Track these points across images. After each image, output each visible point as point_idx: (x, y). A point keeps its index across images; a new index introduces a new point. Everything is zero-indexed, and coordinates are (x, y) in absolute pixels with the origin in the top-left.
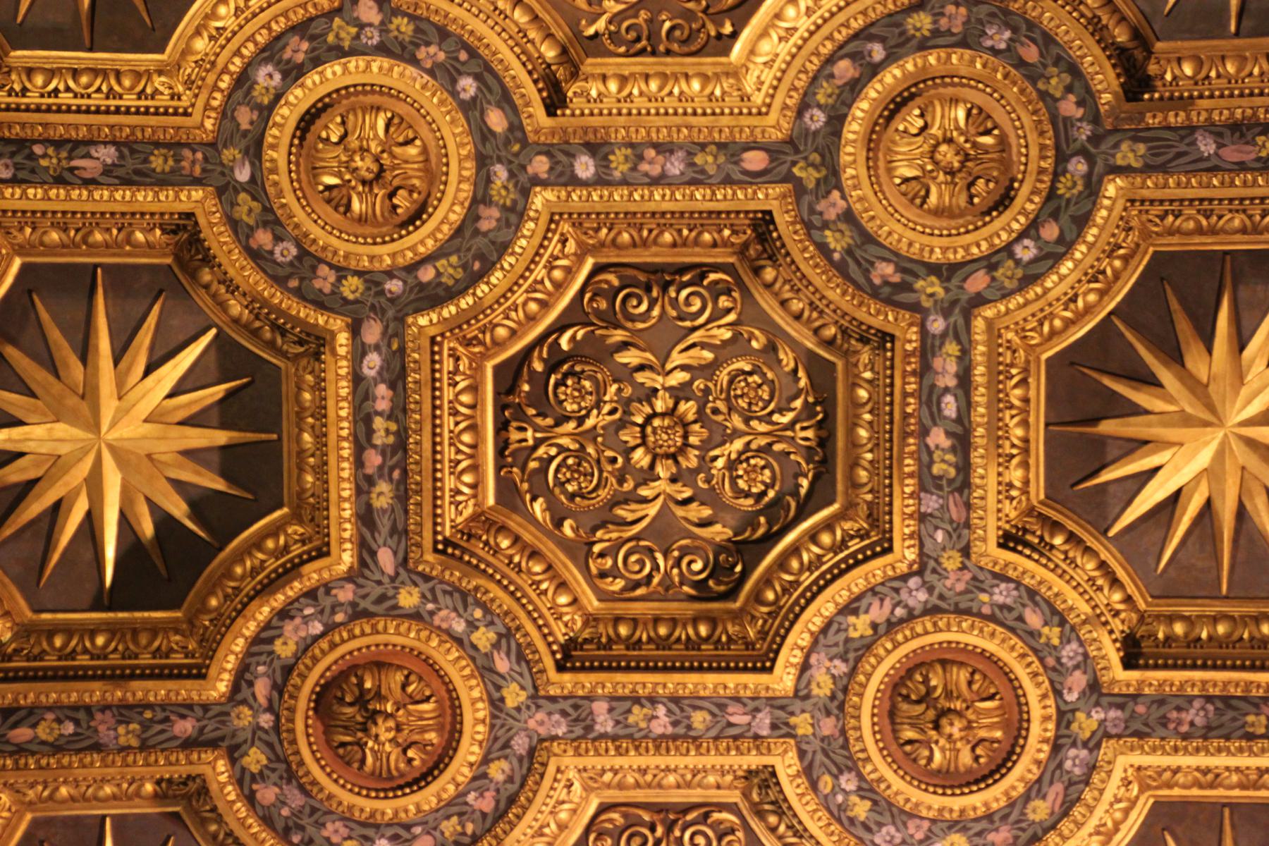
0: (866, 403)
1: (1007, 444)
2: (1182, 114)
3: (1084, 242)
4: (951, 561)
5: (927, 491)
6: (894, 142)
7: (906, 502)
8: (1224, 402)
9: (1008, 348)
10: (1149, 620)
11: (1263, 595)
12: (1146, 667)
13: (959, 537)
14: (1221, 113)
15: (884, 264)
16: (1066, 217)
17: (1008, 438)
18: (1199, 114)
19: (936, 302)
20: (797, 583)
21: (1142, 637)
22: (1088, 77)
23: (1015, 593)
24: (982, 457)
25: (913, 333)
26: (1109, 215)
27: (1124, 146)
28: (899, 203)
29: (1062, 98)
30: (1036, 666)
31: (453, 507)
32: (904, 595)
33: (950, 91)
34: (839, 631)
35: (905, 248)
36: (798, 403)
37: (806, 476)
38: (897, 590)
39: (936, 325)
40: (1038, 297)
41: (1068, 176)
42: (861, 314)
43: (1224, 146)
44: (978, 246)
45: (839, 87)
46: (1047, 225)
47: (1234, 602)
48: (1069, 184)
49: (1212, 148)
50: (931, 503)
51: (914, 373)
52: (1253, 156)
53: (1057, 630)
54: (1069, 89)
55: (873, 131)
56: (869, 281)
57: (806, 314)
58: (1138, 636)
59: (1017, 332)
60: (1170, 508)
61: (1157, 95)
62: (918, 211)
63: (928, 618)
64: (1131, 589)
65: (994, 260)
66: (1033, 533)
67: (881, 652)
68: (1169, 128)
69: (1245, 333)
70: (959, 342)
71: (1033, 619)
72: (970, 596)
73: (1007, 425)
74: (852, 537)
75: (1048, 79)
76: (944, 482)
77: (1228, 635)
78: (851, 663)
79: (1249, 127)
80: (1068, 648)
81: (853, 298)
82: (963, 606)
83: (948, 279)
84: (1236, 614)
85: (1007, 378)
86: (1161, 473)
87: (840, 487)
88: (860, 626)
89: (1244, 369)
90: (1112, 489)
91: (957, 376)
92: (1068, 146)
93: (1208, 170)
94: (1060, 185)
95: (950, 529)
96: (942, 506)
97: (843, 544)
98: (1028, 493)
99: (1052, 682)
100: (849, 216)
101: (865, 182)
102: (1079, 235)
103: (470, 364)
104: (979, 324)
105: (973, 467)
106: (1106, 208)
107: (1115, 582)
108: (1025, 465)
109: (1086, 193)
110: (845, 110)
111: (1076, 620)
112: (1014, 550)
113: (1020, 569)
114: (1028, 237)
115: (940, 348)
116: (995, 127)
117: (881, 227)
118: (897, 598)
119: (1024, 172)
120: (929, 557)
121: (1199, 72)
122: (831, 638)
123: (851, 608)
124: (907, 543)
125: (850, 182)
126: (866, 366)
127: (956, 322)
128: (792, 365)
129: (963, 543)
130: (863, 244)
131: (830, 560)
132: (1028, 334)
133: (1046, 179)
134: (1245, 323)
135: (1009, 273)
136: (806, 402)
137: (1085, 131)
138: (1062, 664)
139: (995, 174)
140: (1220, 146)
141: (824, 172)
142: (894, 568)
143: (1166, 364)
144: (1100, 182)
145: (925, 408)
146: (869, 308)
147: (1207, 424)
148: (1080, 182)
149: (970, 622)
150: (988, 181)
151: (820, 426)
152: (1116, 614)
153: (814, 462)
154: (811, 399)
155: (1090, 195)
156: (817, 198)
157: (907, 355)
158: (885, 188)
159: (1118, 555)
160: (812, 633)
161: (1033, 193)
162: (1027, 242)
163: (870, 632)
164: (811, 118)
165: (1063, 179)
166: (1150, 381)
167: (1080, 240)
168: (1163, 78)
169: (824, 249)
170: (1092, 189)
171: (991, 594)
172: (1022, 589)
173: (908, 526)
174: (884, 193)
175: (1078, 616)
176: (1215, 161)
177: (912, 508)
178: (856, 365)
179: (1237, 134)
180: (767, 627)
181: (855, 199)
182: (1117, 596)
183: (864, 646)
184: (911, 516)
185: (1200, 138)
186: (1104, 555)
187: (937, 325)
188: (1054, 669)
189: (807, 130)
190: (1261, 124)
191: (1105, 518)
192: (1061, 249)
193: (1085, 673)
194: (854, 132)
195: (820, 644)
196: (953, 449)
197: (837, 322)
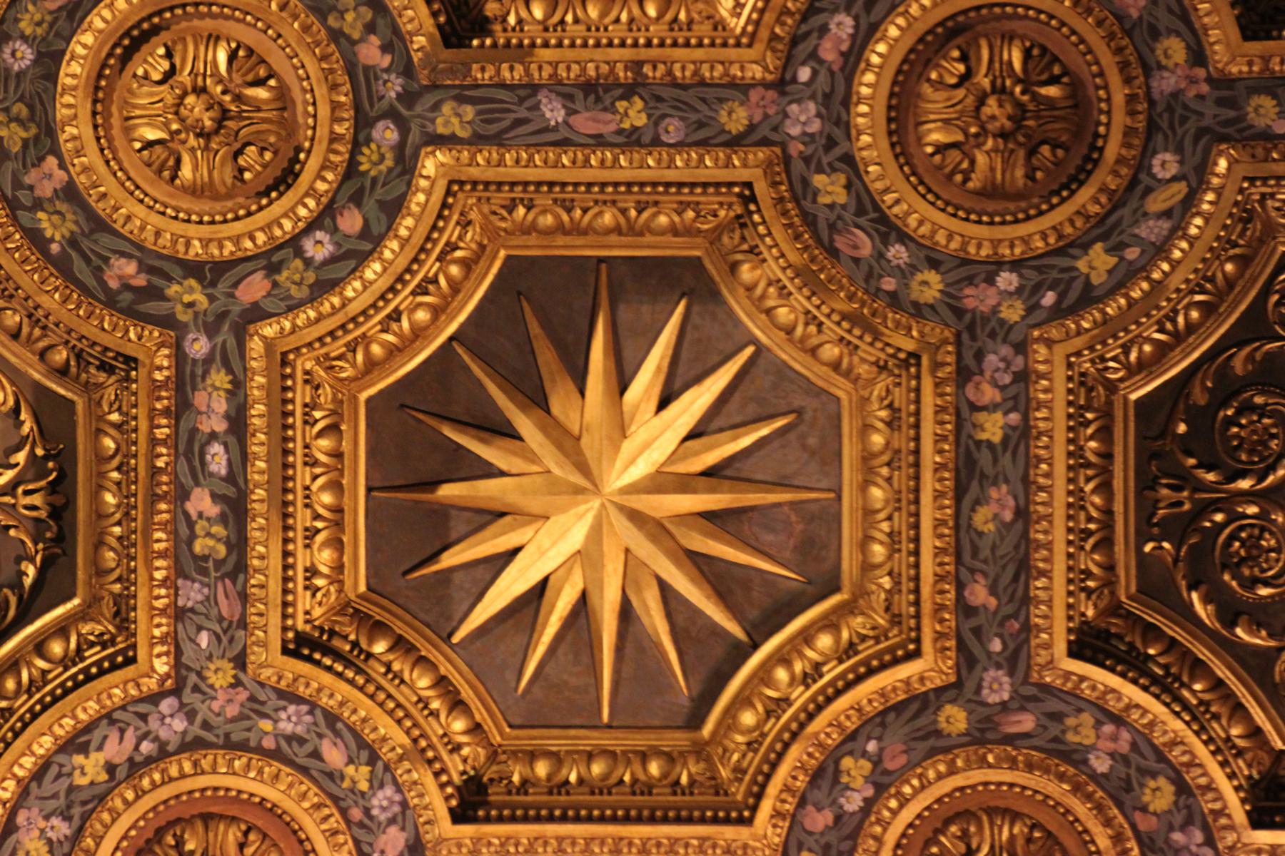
0: (113, 457)
1: (1082, 516)
2: (519, 69)
3: (396, 236)
4: (220, 674)
5: (186, 577)
6: (131, 92)
7: (157, 592)
8: (600, 460)
9: (1082, 384)
10: (503, 757)
11: (657, 723)
12: (487, 820)
13: (231, 641)
14: (569, 68)
15: (123, 260)
16: (372, 201)
17: (1083, 508)
18: (540, 68)
19: (196, 314)
20: (786, 701)
21: (491, 780)
22: (395, 13)
23: (308, 719)
24: (261, 529)
25: (163, 358)
26: (427, 201)
27: (447, 108)
28: (143, 176)
29: (362, 40)
30: (335, 821)
31: (308, 593)
32: (153, 724)
33: (208, 24)
34: (59, 776)
35: (151, 239)
36: (21, 457)
37: (32, 560)
38: (144, 717)
39: (196, 346)
40: (334, 311)
41: (373, 146)
42: (90, 330)
43: (576, 112)
44: (253, 239)
45: (51, 13)
46: (346, 213)
47: (619, 734)
48: (375, 157)
49: (560, 115)
50: (192, 594)
51: (166, 412)
52: (613, 127)
53: (365, 770)
54: (370, 28)
55: (100, 76)
56: (103, 283)
57: (25, 330)
58: (485, 779)
59: (1092, 361)
60: (534, 605)
61: (488, 42)
62: (170, 189)
63: (187, 755)
64: (480, 715)
65: (275, 259)
66: (345, 637)
67: (118, 803)
68: (503, 86)
69: (628, 369)
70: (230, 371)
71: (334, 755)
72: (247, 723)
73: (1082, 490)
74: (92, 645)
75: (342, 14)
76: (211, 564)
77: (605, 777)
78: (76, 822)
79: (607, 89)
80: (380, 794)
81: (78, 307)
82: (235, 737)
83: (213, 284)
84: (618, 749)
85: (1081, 424)
86: (520, 556)
87: (81, 574)
88: (90, 768)
89: (626, 417)
90: (458, 578)
91: (227, 416)
92: (372, 106)
93: (555, 144)
94: (362, 159)
95: (219, 630)
96: (208, 598)
97: (851, 649)
98: (341, 582)
99: (357, 842)
100: (70, 192)
101: (91, 147)
102: (389, 228)
103: (334, 395)
104: (255, 346)
105: (251, 543)
106: (423, 191)
107: (457, 704)
108: (337, 544)
109: (399, 169)
110: (60, 45)
111: (390, 755)
112: (309, 659)
113: (315, 685)
114: (321, 228)
115: (203, 379)
116: (270, 77)
117: (116, 209)
118: (144, 729)
119: (312, 139)
120: (189, 669)
121: (552, 15)
122: (48, 787)
123: (77, 743)
124: (158, 649)
125: (69, 145)
126: (111, 405)
127: (224, 342)
128: (11, 402)
129: (237, 649)
130: (92, 231)
131: (59, 677)
132: (335, 363)
133: (341, 148)
134: (628, 353)
135: (297, 277)
136: (32, 455)
137: (393, 87)
138: (371, 818)
139: (272, 139)
140: (571, 112)
141: (34, 131)
142: (138, 685)
143: (523, 408)
144: (416, 156)
145: (183, 463)
146: (102, 321)
147: (578, 491)
148: (389, 155)
149: (244, 760)
150: (262, 150)
151: (53, 488)
152: (457, 748)
153: (45, 541)
154: (40, 452)
155: (403, 173)
156: (24, 166)
157: (155, 386)
158: (121, 155)
159: (465, 669)
160: (19, 781)
161: (323, 168)
162: (319, 235)
163: (104, 777)
164: (13, 54)
165: (365, 150)
166: (504, 432)
167: (391, 234)
168: (504, 20)
169: (36, 238)
170: (406, 165)
171: (276, 721)
172: (318, 712)
173: (158, 626)
174: (119, 162)
175: (393, 749)
176: (564, 133)
177: (165, 601)
178: (99, 404)
179: (592, 98)
180: (745, 764)
181: (78, 169)
182: (459, 725)
183: (94, 797)
184: (163, 612)
185: (544, 101)
186: (445, 668)
187: (199, 346)
188: (361, 825)
189: (7, 70)
190: (621, 85)
191: (449, 619)
192: (369, 247)
193: (403, 829)
194: (74, 76)
195: (32, 797)
196: (223, 519)
197: (67, 342)
